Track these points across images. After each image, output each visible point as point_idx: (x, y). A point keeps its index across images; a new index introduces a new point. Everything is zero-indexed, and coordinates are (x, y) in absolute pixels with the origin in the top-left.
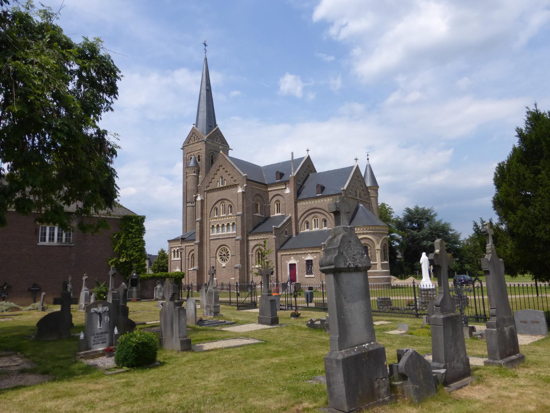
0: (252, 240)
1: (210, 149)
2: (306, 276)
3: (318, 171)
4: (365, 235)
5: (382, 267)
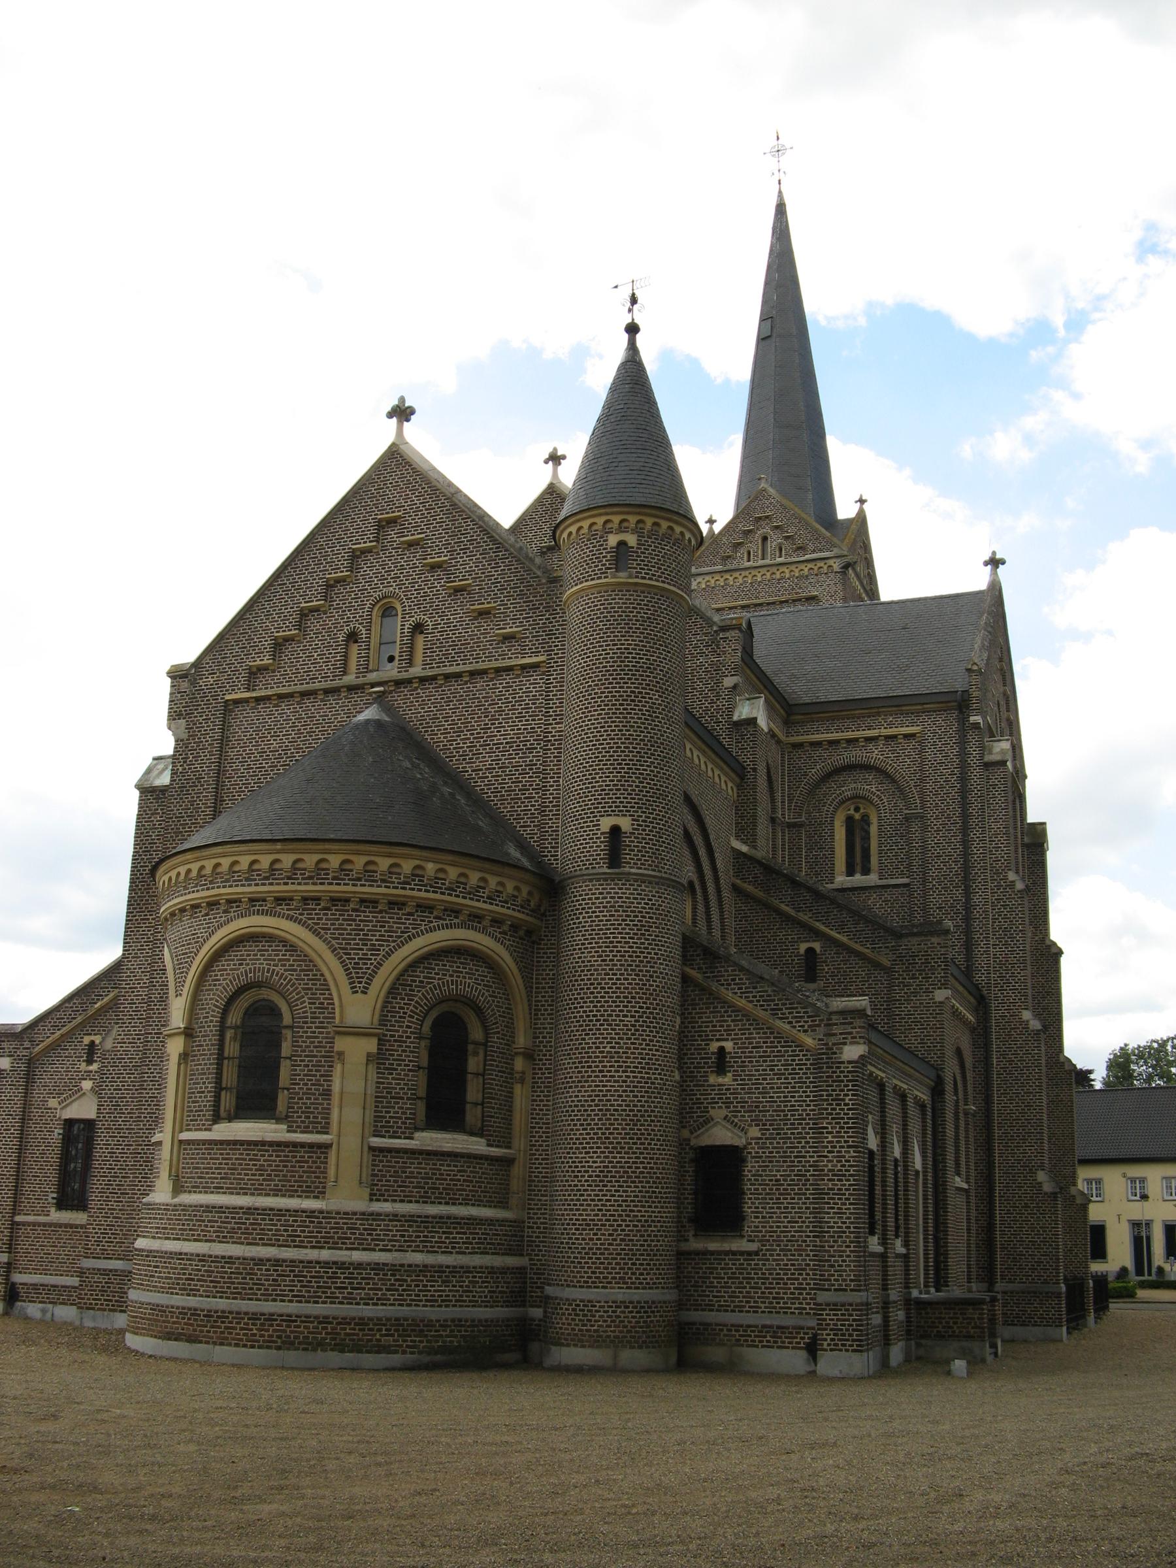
2: (56, 1216)
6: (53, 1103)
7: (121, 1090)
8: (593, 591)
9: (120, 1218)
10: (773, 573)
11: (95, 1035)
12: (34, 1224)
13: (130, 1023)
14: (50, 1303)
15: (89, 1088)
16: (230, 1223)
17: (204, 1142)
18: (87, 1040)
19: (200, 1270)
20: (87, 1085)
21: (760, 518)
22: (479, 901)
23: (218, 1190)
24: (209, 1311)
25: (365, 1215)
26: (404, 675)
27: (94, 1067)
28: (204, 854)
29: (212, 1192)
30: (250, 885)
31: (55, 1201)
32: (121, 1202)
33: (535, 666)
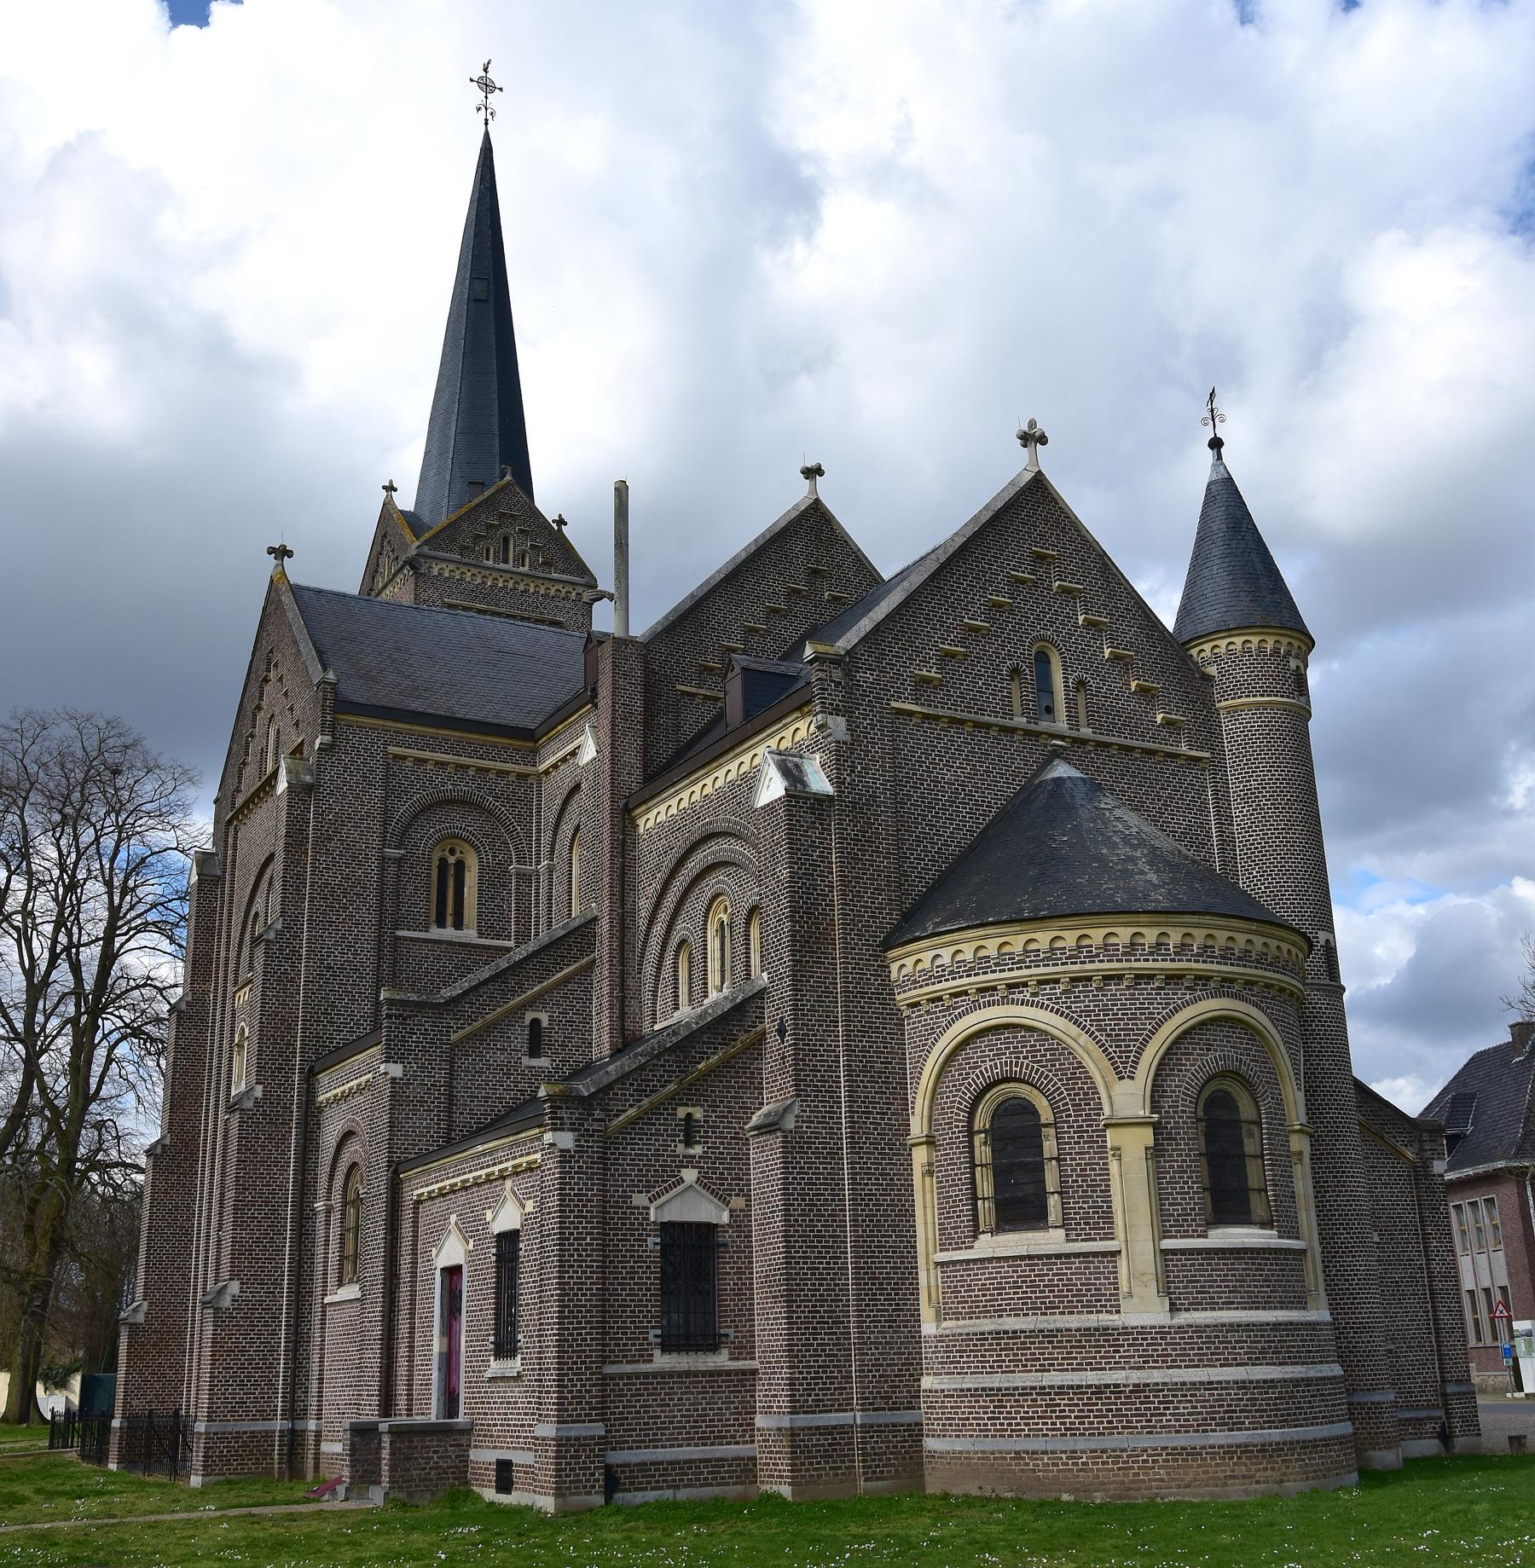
0: (337, 1100)
1: (751, 630)
2: (662, 1361)
3: (886, 577)
4: (1004, 1001)
5: (1166, 1288)
6: (639, 1199)
7: (815, 1184)
8: (1280, 706)
9: (836, 1355)
10: (549, 589)
11: (693, 1106)
12: (629, 1376)
13: (817, 1096)
14: (668, 1487)
15: (695, 1179)
16: (1260, 1342)
17: (1199, 1251)
18: (682, 1112)
19: (1242, 1399)
20: (690, 1175)
21: (504, 514)
22: (986, 973)
23: (1228, 1305)
24: (1262, 1445)
25: (1162, 1331)
26: (1032, 727)
27: (697, 1150)
28: (1170, 920)
29: (1222, 1309)
30: (1226, 964)
31: (659, 1340)
32: (835, 1333)
33: (1199, 759)
